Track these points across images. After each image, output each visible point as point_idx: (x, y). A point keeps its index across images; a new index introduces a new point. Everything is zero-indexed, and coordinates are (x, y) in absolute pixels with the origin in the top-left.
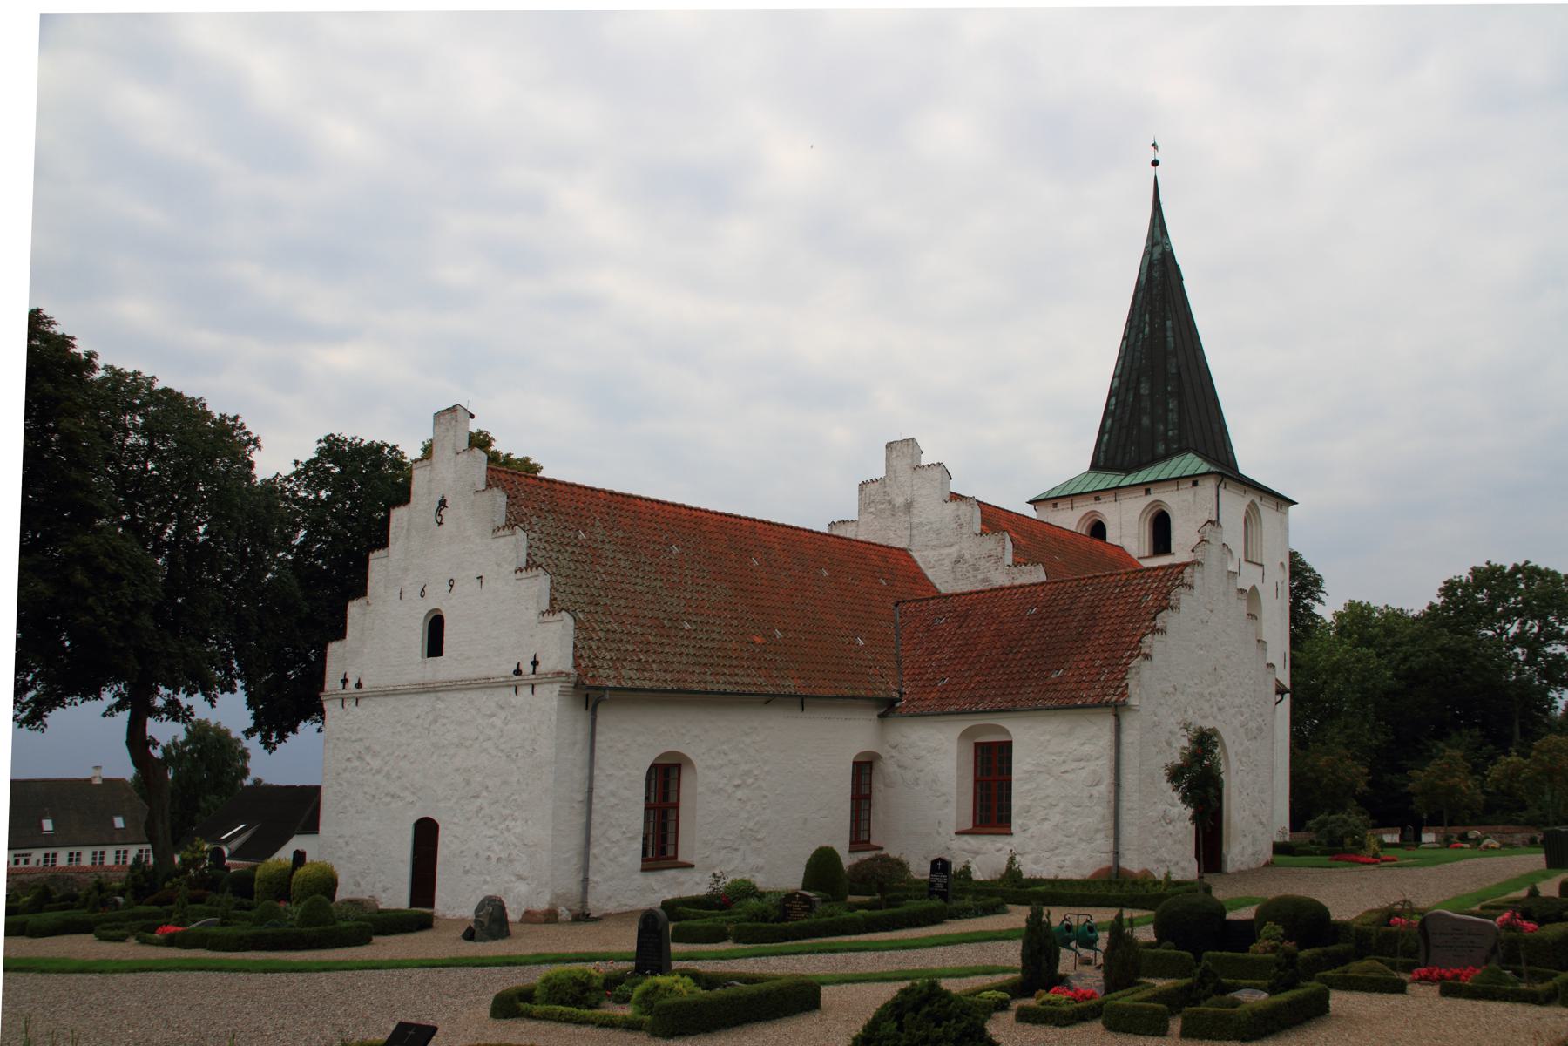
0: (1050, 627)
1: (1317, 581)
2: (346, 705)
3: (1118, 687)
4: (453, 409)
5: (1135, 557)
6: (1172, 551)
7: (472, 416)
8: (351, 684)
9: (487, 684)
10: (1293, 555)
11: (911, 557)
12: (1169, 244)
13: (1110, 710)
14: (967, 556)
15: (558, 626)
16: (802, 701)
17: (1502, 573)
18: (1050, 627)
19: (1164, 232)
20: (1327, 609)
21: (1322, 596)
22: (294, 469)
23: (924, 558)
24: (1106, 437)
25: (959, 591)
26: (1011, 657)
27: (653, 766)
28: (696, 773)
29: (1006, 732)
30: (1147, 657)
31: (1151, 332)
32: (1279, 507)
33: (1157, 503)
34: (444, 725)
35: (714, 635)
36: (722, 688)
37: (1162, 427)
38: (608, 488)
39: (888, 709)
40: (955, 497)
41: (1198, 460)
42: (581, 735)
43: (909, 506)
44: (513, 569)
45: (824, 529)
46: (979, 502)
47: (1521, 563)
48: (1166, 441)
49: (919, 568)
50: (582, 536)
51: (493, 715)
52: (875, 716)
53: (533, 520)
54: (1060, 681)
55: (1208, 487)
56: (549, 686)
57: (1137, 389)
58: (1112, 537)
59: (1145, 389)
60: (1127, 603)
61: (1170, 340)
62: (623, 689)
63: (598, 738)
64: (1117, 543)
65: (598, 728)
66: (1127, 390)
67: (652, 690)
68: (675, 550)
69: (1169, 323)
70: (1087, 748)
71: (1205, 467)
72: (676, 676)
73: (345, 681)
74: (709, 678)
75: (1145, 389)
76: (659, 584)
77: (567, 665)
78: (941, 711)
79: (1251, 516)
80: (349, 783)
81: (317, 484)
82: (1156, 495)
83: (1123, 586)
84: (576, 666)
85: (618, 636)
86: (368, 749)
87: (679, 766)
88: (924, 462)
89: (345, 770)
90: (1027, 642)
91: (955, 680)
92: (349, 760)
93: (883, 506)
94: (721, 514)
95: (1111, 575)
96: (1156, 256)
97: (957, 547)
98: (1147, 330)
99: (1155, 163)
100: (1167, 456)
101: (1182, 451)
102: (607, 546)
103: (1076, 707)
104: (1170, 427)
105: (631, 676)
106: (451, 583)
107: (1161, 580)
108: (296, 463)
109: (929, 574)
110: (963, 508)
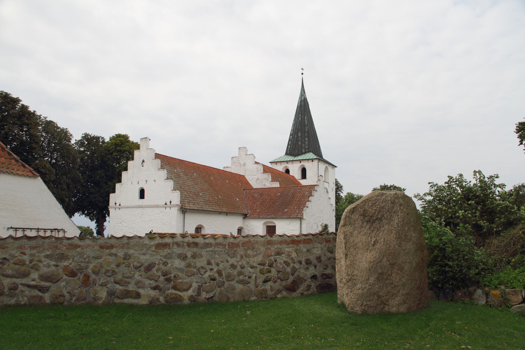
0: (283, 198)
1: (341, 187)
2: (116, 210)
3: (301, 214)
4: (146, 138)
5: (297, 179)
6: (307, 178)
7: (150, 140)
8: (117, 205)
9: (157, 206)
10: (336, 179)
11: (245, 177)
12: (306, 96)
13: (299, 219)
14: (260, 179)
15: (177, 194)
16: (227, 214)
17: (388, 187)
18: (283, 198)
19: (304, 93)
20: (343, 194)
21: (342, 191)
22: (75, 142)
23: (248, 178)
24: (289, 146)
25: (259, 188)
26: (274, 205)
27: (196, 228)
28: (205, 230)
29: (274, 223)
30: (307, 207)
31: (301, 119)
32: (333, 168)
33: (303, 165)
34: (145, 216)
35: (207, 197)
36: (211, 210)
37: (304, 145)
38: (178, 158)
39: (245, 216)
40: (256, 163)
41: (313, 155)
42: (182, 220)
43: (244, 164)
44: (164, 179)
45: (222, 169)
46: (262, 165)
47: (392, 185)
48: (305, 149)
49: (247, 180)
50: (175, 171)
51: (159, 214)
52: (242, 218)
53: (165, 166)
54: (287, 212)
55: (316, 162)
56: (175, 208)
57: (298, 134)
58: (291, 173)
59: (299, 135)
60: (301, 194)
61: (306, 122)
62: (191, 209)
63: (185, 221)
64: (292, 175)
65: (185, 218)
66: (295, 134)
67: (196, 210)
68: (195, 175)
69: (306, 117)
70: (293, 228)
71: (315, 157)
72: (201, 207)
73: (116, 204)
74: (208, 207)
75: (299, 135)
76: (193, 183)
77: (179, 203)
78: (259, 217)
79: (326, 169)
80: (117, 229)
81: (430, 232)
82: (303, 163)
83: (300, 189)
84: (181, 203)
85: (187, 196)
86: (123, 221)
87: (201, 228)
88: (248, 153)
89: (116, 226)
90: (278, 202)
91: (261, 210)
92: (117, 223)
93: (238, 164)
94: (203, 165)
95: (297, 186)
96: (303, 99)
97: (257, 176)
98: (300, 119)
99: (302, 74)
100: (305, 153)
101: (309, 152)
102: (181, 173)
103: (291, 218)
104: (306, 145)
105: (192, 206)
106: (146, 181)
107: (309, 189)
108: (76, 140)
109: (250, 182)
110: (258, 166)
